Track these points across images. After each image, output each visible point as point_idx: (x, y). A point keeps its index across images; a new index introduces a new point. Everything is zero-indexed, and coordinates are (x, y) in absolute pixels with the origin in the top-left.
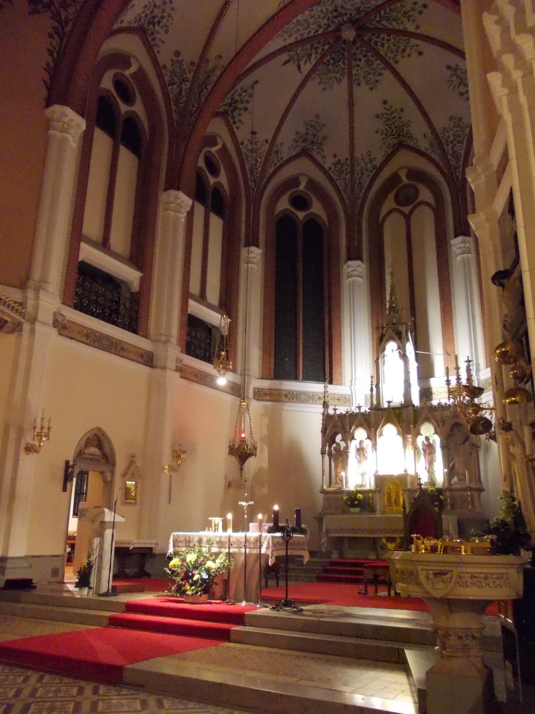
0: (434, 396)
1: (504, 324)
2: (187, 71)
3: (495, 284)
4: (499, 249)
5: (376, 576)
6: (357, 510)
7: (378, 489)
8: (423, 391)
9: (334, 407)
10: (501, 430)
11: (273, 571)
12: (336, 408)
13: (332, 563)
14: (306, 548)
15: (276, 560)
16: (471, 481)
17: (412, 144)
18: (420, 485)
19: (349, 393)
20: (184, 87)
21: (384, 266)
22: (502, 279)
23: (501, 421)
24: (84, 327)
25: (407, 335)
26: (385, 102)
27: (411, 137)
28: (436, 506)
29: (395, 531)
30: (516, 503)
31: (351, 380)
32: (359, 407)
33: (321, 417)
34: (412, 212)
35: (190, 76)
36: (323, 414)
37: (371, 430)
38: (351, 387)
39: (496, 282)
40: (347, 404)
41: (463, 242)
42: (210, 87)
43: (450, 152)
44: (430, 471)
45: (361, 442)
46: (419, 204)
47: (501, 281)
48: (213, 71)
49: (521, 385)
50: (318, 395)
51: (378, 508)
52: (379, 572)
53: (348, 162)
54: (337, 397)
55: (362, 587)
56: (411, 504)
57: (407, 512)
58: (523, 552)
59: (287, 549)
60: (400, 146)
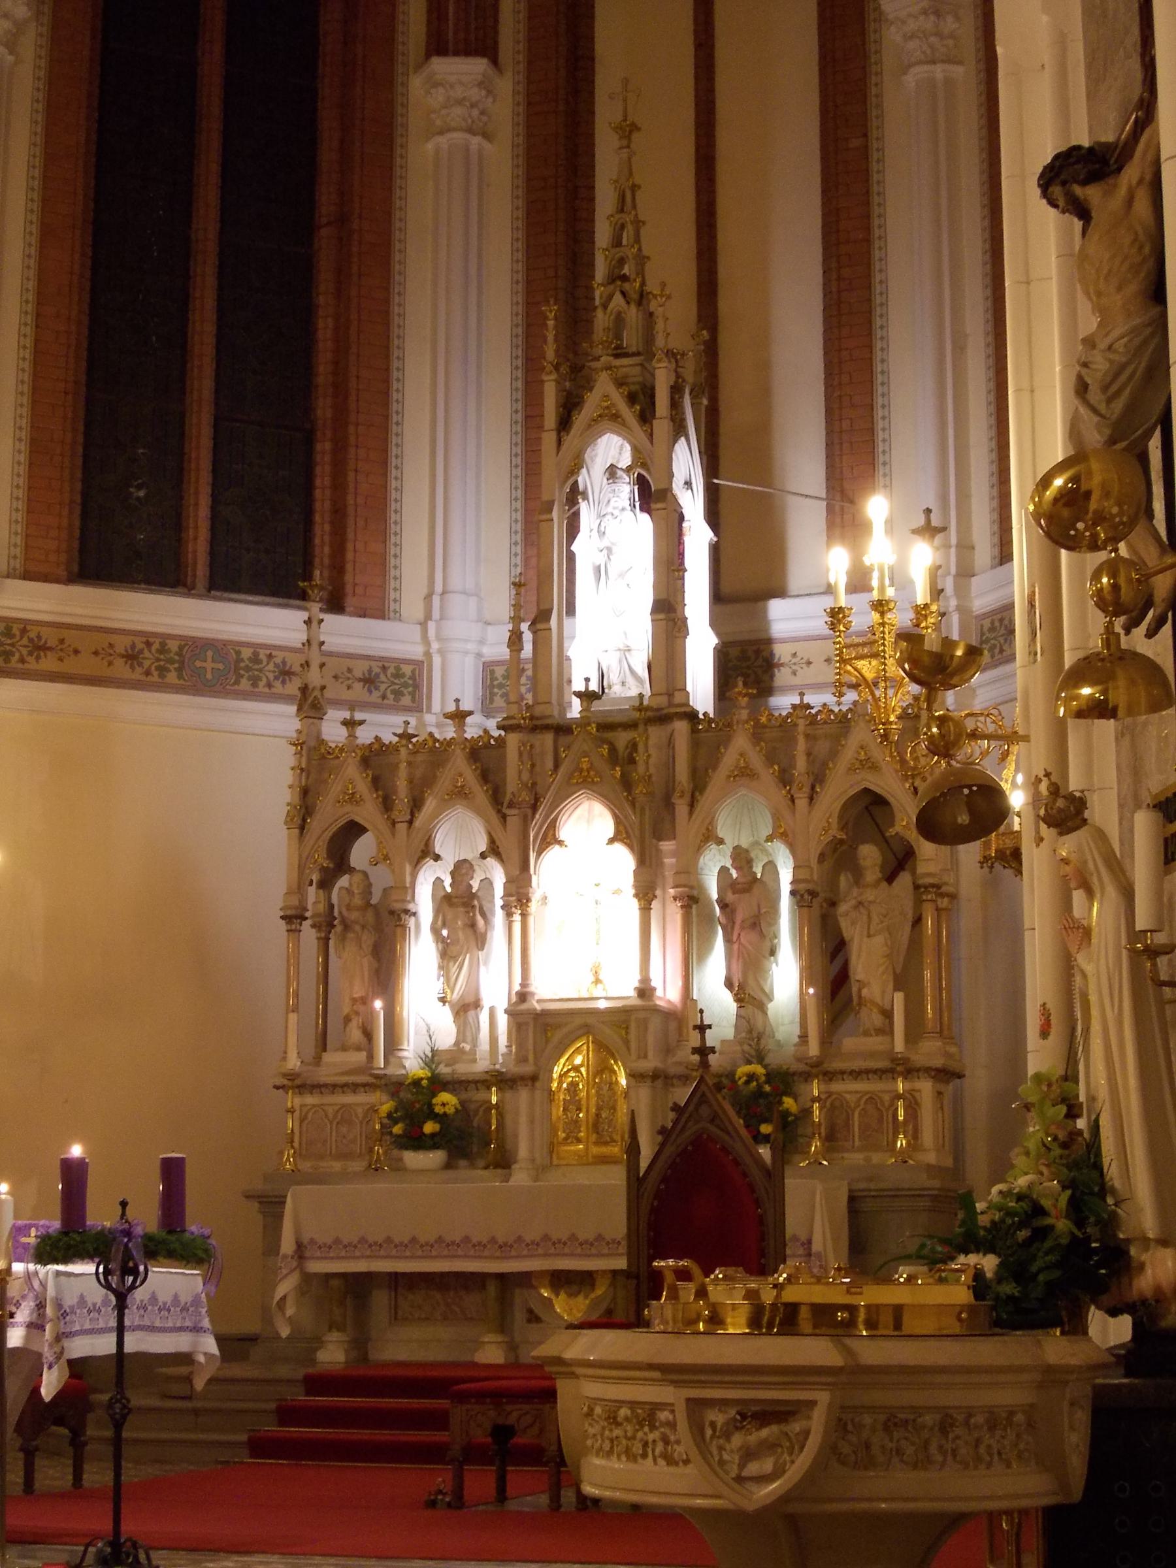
0: (782, 677)
1: (1080, 378)
3: (1053, 204)
4: (1077, 52)
5: (502, 1433)
6: (434, 1158)
7: (528, 1069)
8: (734, 652)
9: (347, 715)
10: (1043, 826)
11: (59, 1422)
12: (359, 716)
13: (318, 1383)
14: (206, 1323)
15: (72, 1376)
16: (913, 1034)
18: (703, 1051)
19: (415, 651)
21: (591, 123)
22: (1085, 182)
23: (1043, 788)
25: (675, 404)
28: (766, 1139)
29: (589, 1246)
30: (1081, 1124)
31: (428, 597)
32: (459, 717)
33: (287, 758)
36: (298, 744)
37: (504, 817)
38: (424, 625)
39: (1057, 191)
40: (406, 700)
45: (461, 870)
47: (1078, 190)
49: (1138, 641)
50: (279, 657)
51: (523, 1152)
52: (515, 1414)
54: (360, 669)
55: (441, 1478)
56: (663, 1131)
57: (644, 1164)
58: (1096, 1318)
59: (121, 1330)
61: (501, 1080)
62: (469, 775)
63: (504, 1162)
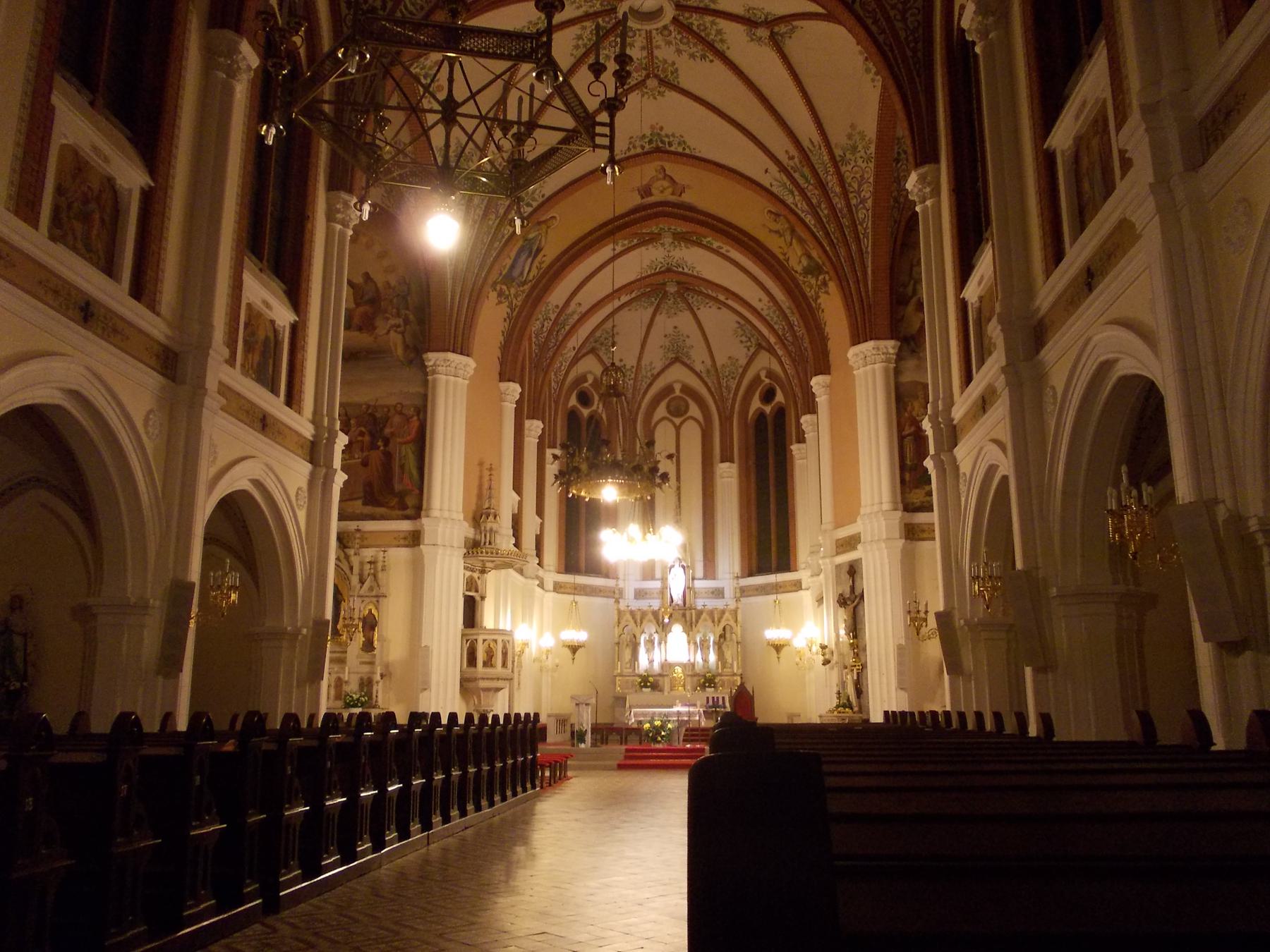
2: (551, 312)
17: (688, 362)
20: (546, 324)
24: (399, 531)
26: (675, 327)
27: (689, 357)
34: (682, 423)
35: (553, 317)
41: (730, 467)
42: (567, 328)
43: (725, 385)
44: (705, 660)
46: (688, 418)
48: (572, 315)
53: (634, 370)
60: (677, 360)
61: (660, 675)
62: (652, 618)
63: (661, 690)
